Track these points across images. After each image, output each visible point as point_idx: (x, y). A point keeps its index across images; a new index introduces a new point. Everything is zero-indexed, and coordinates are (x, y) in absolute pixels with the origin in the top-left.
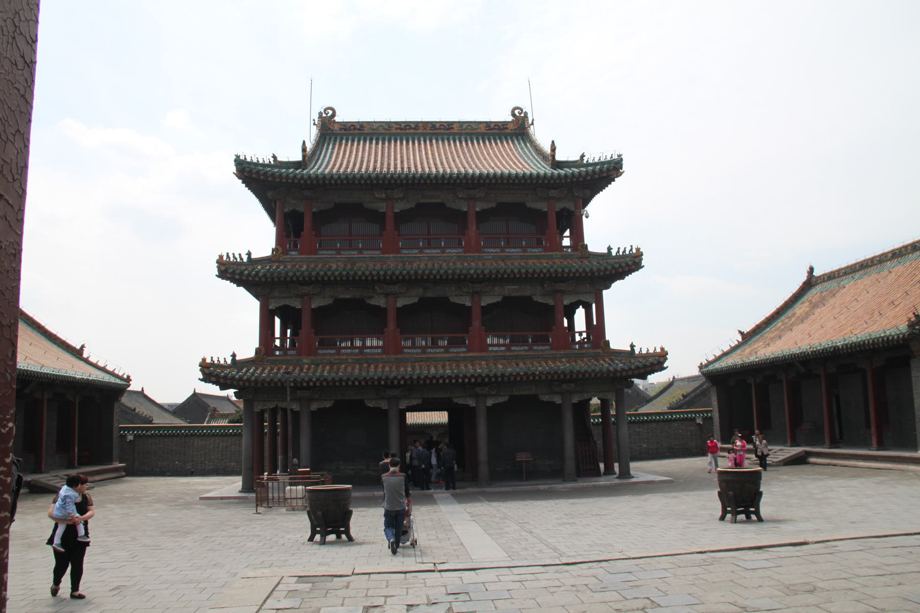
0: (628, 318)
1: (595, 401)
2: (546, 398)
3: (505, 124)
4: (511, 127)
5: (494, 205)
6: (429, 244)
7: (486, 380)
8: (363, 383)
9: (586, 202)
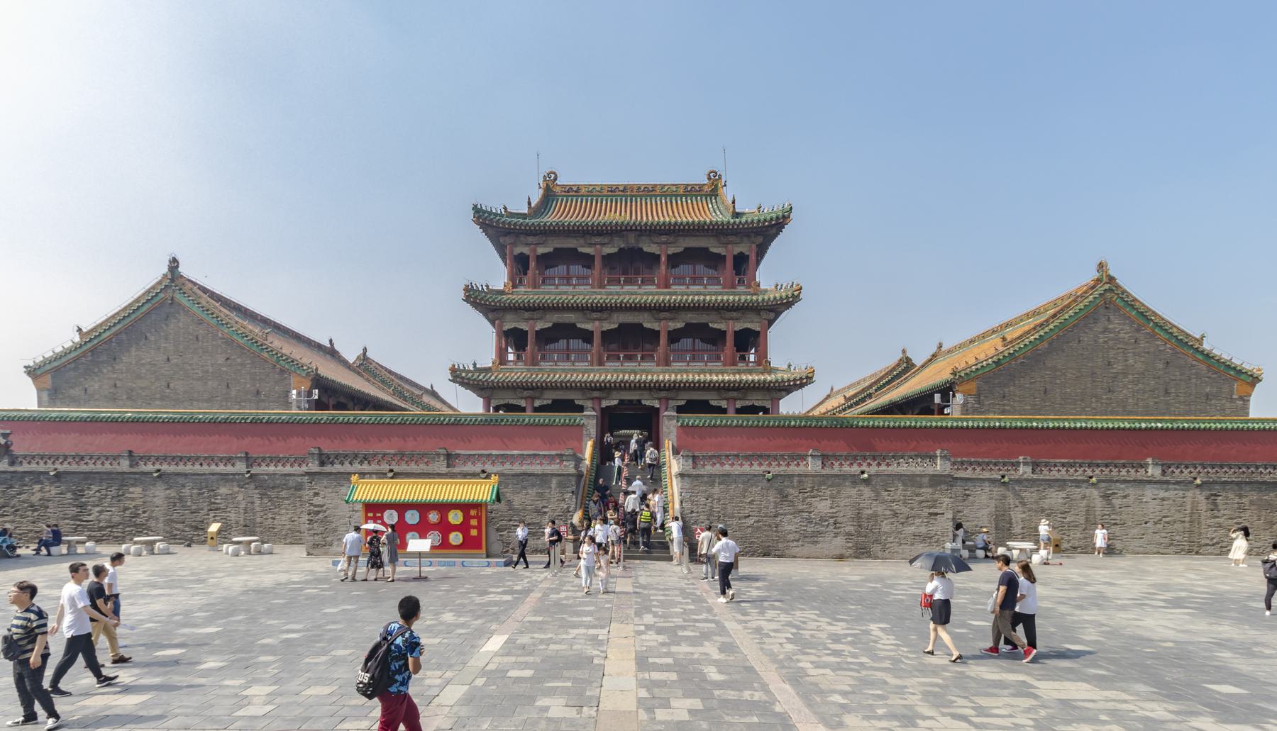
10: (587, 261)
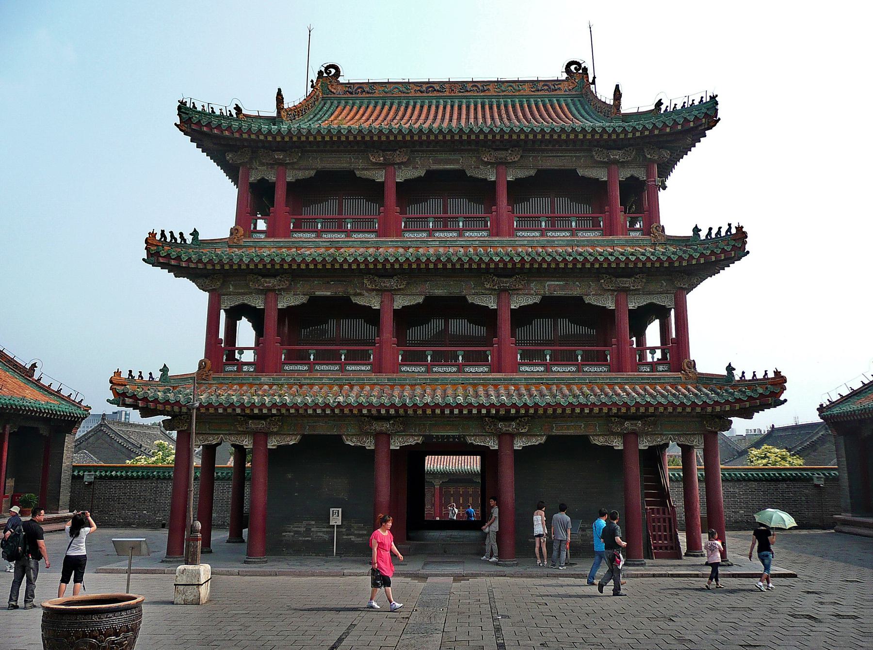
0: (724, 328)
1: (674, 451)
2: (599, 441)
3: (558, 81)
4: (565, 86)
5: (532, 173)
6: (445, 225)
7: (513, 411)
8: (337, 411)
9: (666, 169)
10: (373, 191)
